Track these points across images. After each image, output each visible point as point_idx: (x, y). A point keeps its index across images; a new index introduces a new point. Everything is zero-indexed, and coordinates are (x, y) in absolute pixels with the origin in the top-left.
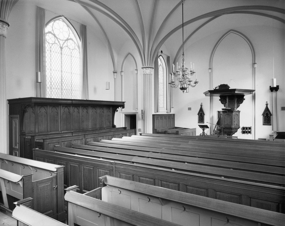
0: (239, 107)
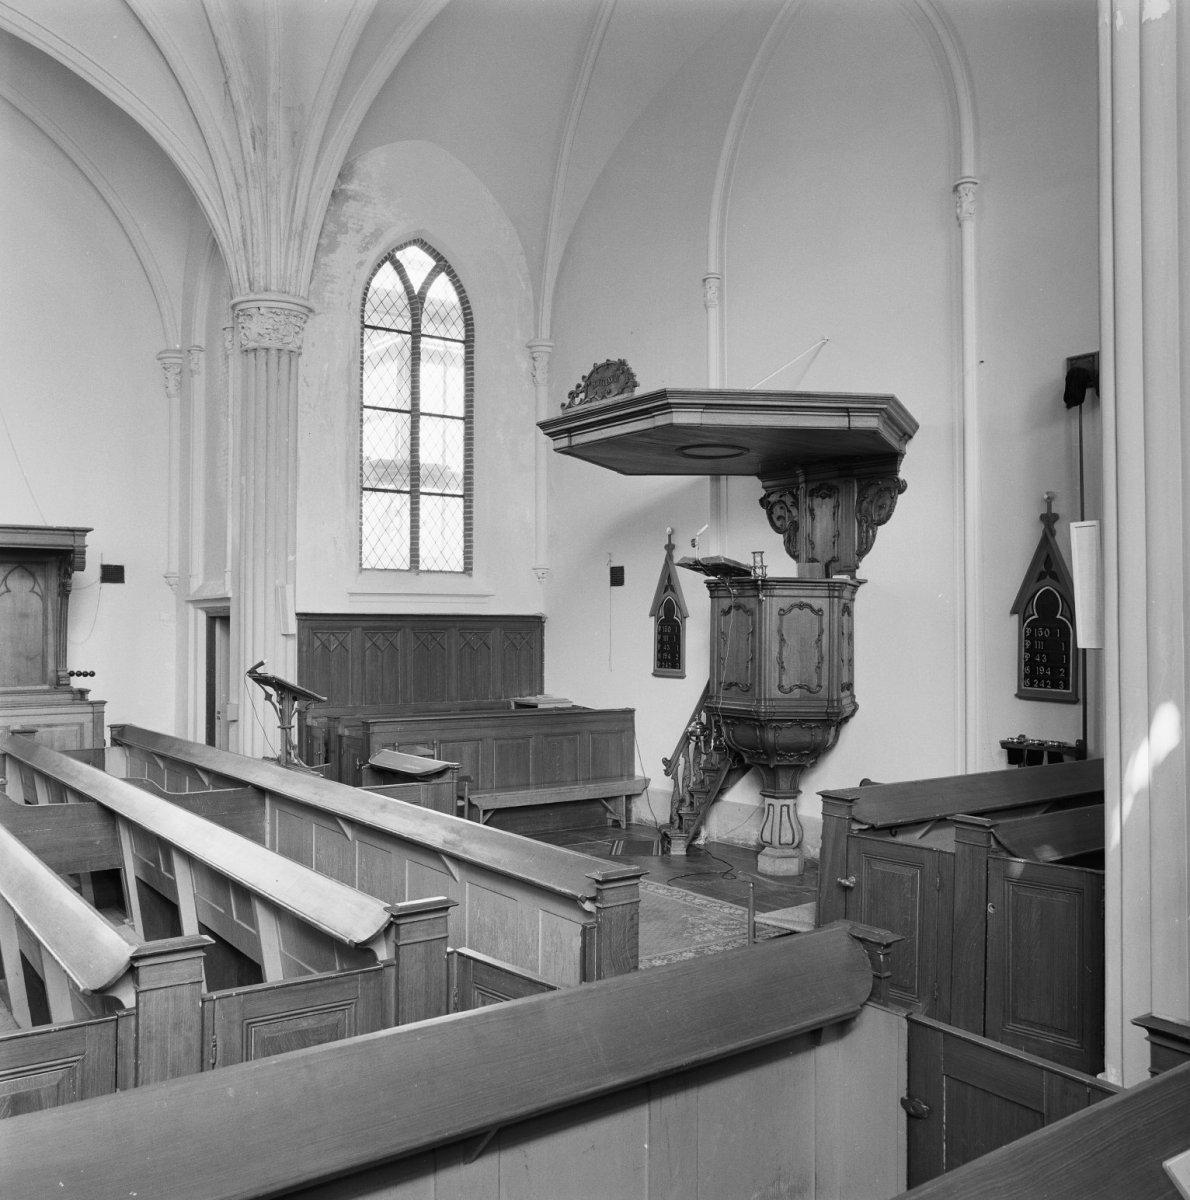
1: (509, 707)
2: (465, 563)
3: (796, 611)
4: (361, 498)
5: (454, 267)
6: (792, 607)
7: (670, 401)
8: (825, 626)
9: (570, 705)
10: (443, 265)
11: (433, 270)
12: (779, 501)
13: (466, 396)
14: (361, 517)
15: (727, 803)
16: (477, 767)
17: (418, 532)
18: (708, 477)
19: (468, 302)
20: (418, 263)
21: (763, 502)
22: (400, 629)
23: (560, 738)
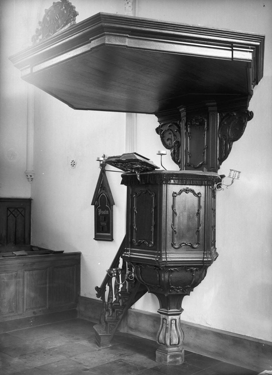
3: (184, 193)
6: (181, 191)
18: (125, 113)
21: (158, 130)
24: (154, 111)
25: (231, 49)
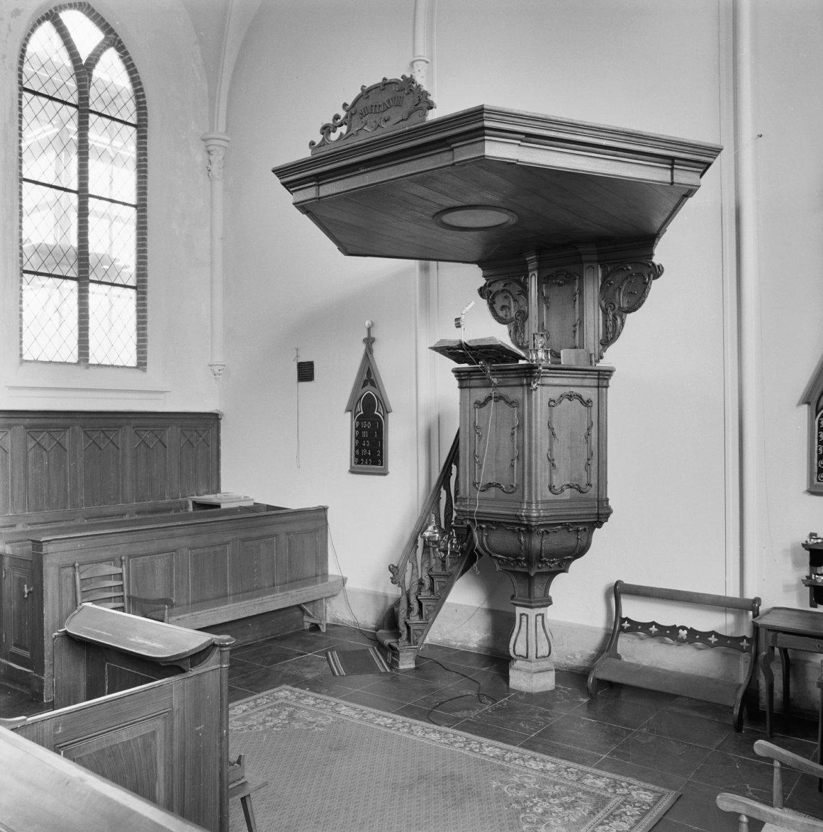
0: (614, 339)
1: (187, 506)
2: (139, 358)
3: (566, 401)
4: (21, 281)
5: (125, 42)
7: (487, 124)
8: (595, 420)
9: (250, 504)
10: (113, 39)
11: (93, 66)
12: (503, 291)
13: (139, 183)
14: (21, 302)
15: (451, 605)
16: (172, 581)
17: (87, 323)
18: (417, 262)
19: (140, 83)
20: (86, 35)
21: (482, 292)
22: (69, 428)
23: (257, 542)
24: (475, 260)
25: (670, 167)
